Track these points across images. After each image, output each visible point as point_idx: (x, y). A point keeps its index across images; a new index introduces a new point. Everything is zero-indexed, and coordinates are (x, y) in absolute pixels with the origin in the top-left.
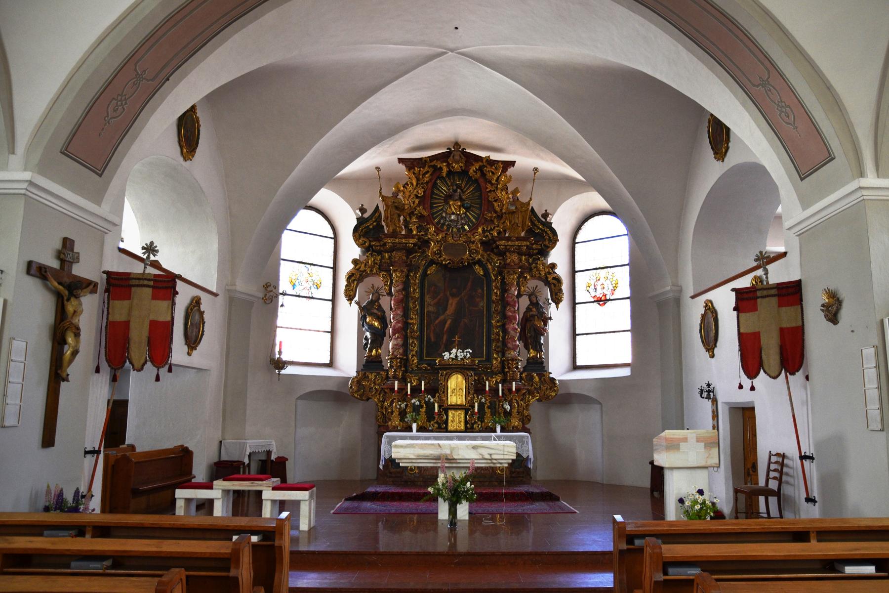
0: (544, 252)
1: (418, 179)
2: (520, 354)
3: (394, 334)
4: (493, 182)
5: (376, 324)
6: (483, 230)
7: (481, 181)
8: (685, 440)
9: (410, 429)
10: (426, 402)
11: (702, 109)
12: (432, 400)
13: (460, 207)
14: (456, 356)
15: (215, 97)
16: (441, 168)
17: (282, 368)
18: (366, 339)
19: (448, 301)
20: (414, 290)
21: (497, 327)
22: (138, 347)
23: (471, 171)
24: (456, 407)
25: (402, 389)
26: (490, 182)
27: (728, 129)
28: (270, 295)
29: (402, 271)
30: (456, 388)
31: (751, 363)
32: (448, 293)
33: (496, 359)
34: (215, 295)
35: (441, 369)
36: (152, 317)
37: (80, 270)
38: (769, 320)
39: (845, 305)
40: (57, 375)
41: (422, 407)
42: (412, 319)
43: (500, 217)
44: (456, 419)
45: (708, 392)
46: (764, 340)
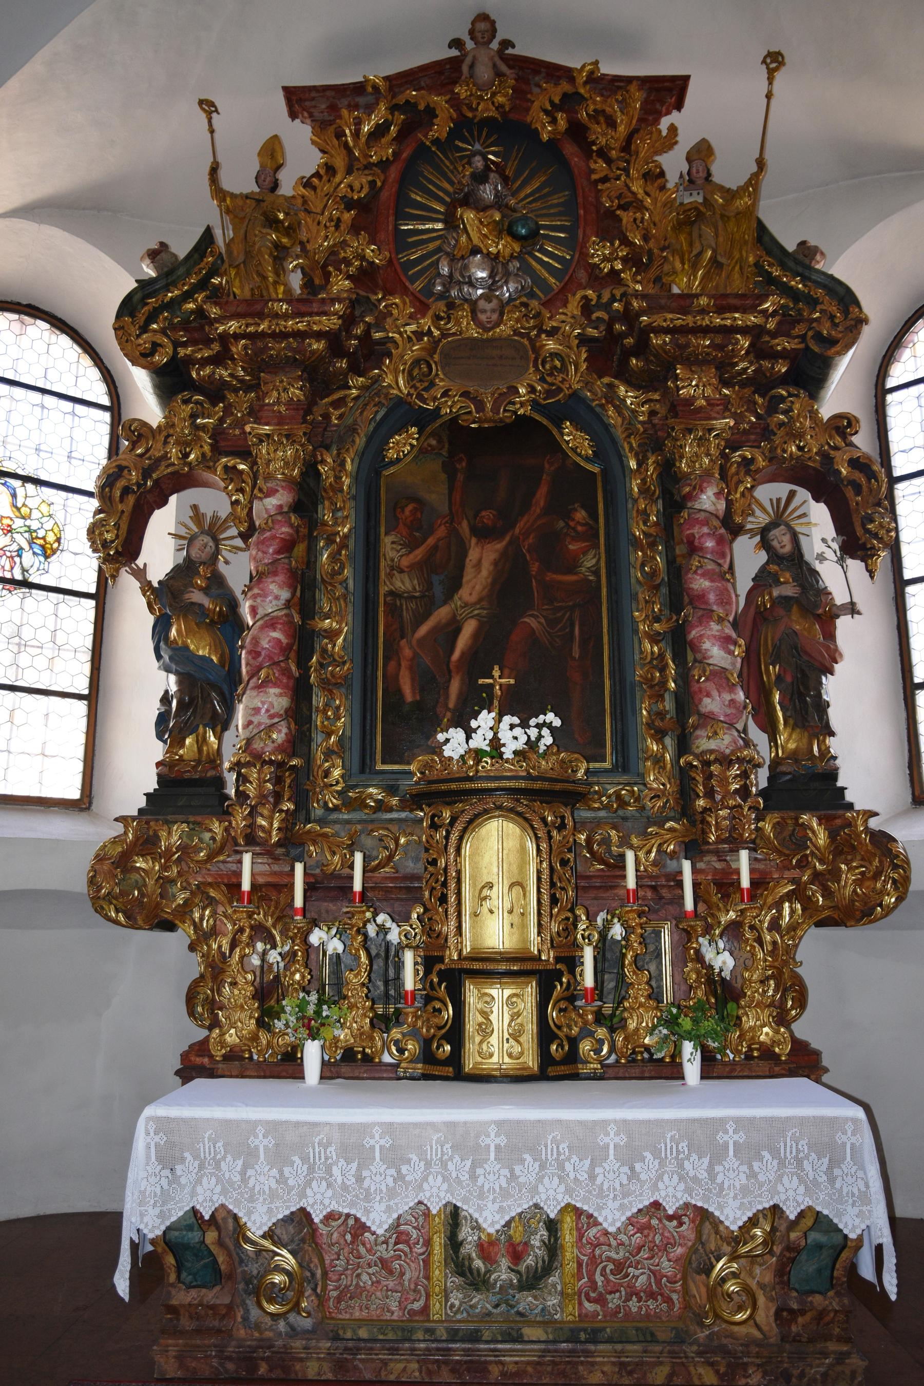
0: (810, 375)
2: (742, 739)
5: (214, 658)
7: (570, 150)
9: (288, 1065)
12: (394, 936)
14: (496, 743)
25: (272, 891)
30: (498, 879)
32: (464, 528)
33: (658, 761)
44: (500, 1020)
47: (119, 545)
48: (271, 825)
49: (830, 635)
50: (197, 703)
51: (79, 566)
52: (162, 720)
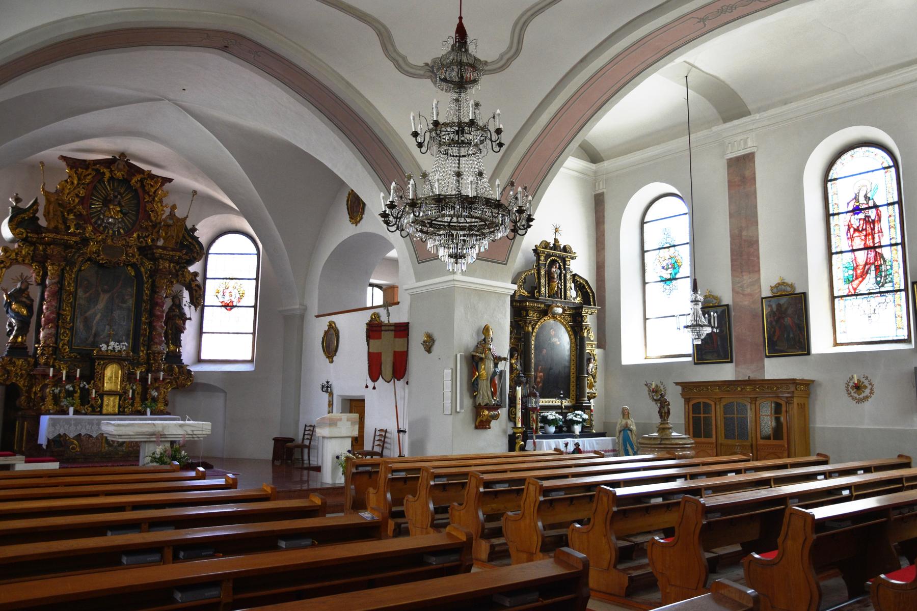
1: (79, 179)
3: (47, 323)
6: (138, 235)
7: (140, 191)
9: (144, 413)
10: (80, 388)
11: (342, 184)
16: (104, 173)
18: (11, 325)
20: (69, 283)
21: (145, 323)
23: (133, 181)
24: (111, 393)
26: (148, 193)
27: (364, 204)
29: (59, 265)
31: (375, 372)
35: (98, 359)
38: (387, 345)
39: (436, 343)
41: (76, 392)
42: (65, 310)
44: (111, 403)
45: (327, 388)
46: (383, 358)
49: (184, 324)
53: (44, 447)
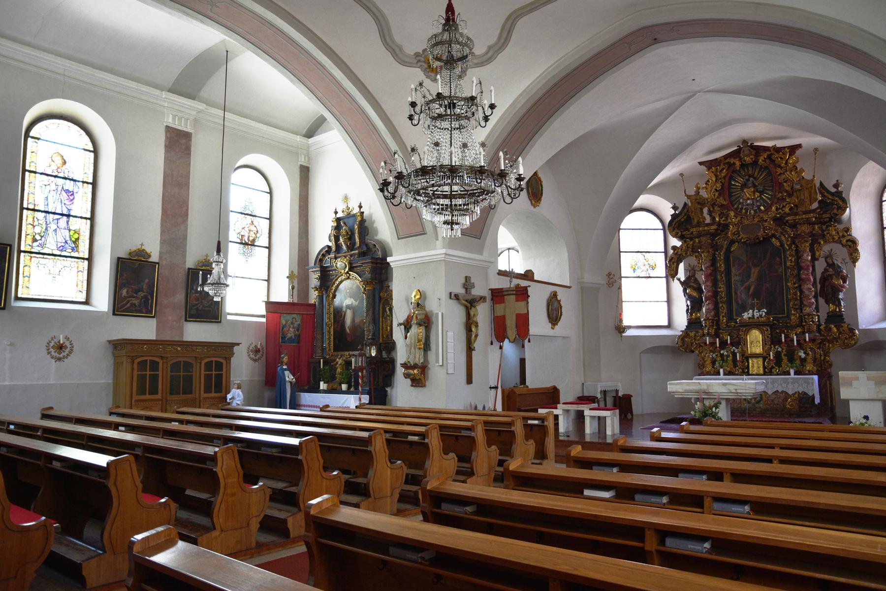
1: (716, 176)
4: (783, 165)
6: (777, 209)
7: (772, 167)
8: (857, 379)
9: (718, 374)
13: (754, 192)
14: (753, 315)
15: (551, 163)
16: (734, 163)
17: (623, 332)
19: (750, 270)
21: (794, 288)
22: (511, 331)
25: (713, 344)
28: (613, 280)
29: (708, 252)
30: (755, 341)
34: (569, 287)
36: (517, 312)
37: (476, 292)
40: (470, 349)
43: (790, 195)
44: (756, 365)
47: (671, 272)
48: (712, 331)
50: (695, 306)
51: (661, 270)
52: (687, 310)
53: (817, 401)
